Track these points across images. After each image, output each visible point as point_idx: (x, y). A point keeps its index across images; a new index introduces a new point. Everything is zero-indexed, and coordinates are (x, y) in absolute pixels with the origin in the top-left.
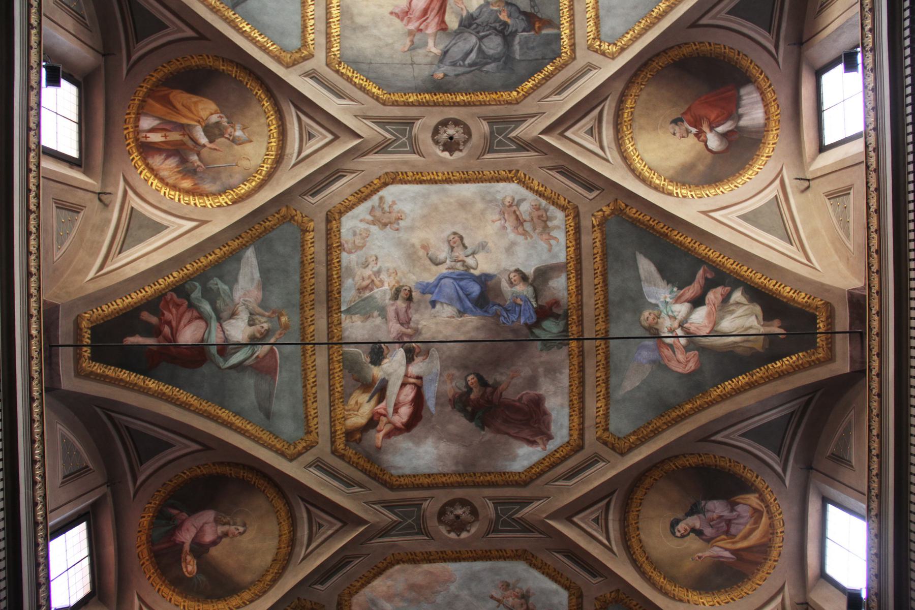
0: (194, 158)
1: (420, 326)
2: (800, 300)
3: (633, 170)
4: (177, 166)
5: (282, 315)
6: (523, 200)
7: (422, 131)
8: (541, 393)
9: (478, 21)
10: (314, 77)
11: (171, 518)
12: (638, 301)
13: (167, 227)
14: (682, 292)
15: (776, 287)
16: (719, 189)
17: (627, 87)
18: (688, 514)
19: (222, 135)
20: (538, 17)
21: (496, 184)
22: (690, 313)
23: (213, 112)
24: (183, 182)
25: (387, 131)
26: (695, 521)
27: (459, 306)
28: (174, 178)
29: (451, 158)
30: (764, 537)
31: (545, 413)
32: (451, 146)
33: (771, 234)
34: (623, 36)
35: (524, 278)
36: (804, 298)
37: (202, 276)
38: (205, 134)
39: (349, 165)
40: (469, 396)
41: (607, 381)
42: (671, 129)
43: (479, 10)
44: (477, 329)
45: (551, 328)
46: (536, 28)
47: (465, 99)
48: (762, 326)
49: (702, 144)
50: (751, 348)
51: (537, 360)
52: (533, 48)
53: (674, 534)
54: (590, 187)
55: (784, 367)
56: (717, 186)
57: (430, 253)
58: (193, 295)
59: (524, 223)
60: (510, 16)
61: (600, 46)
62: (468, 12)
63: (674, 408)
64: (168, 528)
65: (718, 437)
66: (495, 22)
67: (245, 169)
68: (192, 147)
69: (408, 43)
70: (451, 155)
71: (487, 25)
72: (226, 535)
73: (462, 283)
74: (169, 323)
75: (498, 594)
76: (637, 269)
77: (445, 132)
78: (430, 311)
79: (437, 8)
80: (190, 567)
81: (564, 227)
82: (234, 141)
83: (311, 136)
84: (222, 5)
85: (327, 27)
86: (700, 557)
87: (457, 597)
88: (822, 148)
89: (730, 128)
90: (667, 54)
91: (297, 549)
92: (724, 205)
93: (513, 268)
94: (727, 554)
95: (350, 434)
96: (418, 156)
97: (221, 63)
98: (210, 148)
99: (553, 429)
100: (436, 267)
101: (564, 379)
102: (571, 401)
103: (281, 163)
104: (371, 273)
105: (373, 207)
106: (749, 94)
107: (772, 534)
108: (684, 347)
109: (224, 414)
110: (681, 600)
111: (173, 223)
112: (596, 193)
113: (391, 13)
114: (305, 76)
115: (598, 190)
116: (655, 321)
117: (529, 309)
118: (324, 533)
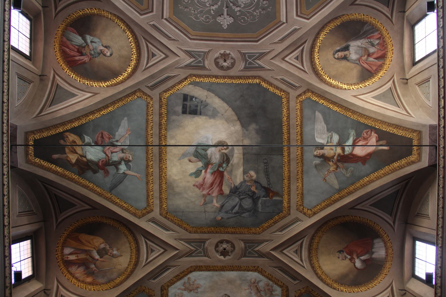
0: (93, 266)
3: (317, 274)
4: (84, 271)
6: (260, 281)
7: (210, 245)
9: (240, 190)
10: (154, 221)
16: (360, 289)
17: (316, 232)
19: (107, 254)
20: (271, 190)
21: (247, 272)
23: (101, 243)
24: (87, 279)
29: (224, 259)
32: (224, 253)
34: (315, 207)
39: (172, 263)
42: (337, 254)
46: (270, 196)
49: (353, 264)
54: (295, 279)
56: (359, 287)
59: (261, 292)
60: (256, 188)
61: (303, 209)
66: (248, 191)
67: (119, 270)
68: (91, 261)
69: (203, 201)
70: (224, 258)
71: (244, 193)
77: (222, 246)
79: (218, 183)
82: (113, 256)
83: (152, 251)
84: (104, 191)
85: (160, 195)
88: (414, 63)
89: (368, 258)
90: (337, 219)
96: (207, 258)
98: (101, 261)
105: (185, 283)
113: (194, 185)
114: (149, 222)
115: (299, 280)
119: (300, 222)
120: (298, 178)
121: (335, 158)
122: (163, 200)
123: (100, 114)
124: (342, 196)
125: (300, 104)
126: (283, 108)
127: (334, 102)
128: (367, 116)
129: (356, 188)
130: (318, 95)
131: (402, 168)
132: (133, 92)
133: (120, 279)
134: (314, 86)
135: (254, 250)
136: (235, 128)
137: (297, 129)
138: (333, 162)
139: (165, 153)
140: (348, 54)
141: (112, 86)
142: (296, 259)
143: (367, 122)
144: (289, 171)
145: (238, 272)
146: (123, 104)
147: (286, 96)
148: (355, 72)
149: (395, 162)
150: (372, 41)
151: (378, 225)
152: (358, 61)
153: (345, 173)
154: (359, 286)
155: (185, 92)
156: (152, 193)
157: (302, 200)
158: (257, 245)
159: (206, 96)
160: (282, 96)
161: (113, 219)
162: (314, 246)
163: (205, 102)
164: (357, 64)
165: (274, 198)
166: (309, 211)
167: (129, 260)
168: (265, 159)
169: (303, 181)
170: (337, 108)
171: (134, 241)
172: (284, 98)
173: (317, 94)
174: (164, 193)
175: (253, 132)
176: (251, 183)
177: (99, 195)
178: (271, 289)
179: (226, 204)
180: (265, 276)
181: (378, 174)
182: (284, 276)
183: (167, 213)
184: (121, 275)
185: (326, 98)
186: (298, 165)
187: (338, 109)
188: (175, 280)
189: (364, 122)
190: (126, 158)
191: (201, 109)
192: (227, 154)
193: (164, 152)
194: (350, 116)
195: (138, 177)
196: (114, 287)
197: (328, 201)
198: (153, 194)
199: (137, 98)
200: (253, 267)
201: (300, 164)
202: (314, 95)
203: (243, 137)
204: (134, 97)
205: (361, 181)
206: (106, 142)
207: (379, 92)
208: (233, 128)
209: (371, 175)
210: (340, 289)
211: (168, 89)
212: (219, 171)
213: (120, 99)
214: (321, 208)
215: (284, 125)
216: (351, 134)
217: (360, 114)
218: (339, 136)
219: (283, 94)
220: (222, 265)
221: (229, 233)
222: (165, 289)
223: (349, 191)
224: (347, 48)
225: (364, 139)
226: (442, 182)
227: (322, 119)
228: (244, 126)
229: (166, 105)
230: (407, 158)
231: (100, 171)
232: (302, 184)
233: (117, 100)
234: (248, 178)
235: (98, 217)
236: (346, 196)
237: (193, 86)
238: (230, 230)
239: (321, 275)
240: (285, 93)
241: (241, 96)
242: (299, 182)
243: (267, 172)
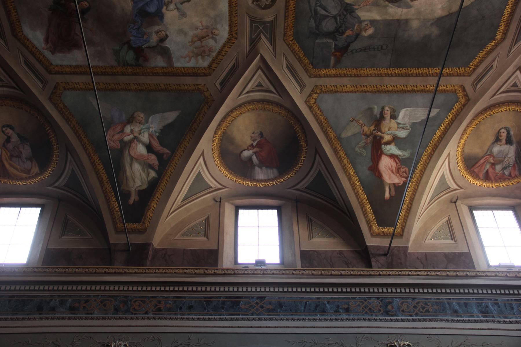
2: (149, 213)
3: (232, 111)
6: (216, 40)
9: (348, 16)
14: (156, 139)
15: (157, 198)
16: (217, 158)
17: (286, 109)
18: (19, 136)
21: (228, 24)
26: (15, 138)
34: (319, 108)
35: (162, 40)
36: (150, 215)
45: (130, 56)
47: (291, 6)
48: (135, 189)
55: (113, 203)
61: (316, 93)
62: (356, 9)
65: (69, 157)
71: (344, 21)
81: (197, 66)
89: (254, 162)
92: (207, 163)
93: (168, 33)
102: (81, 66)
108: (123, 139)
112: (219, 87)
115: (221, 89)
116: (138, 121)
119: (299, 91)
120: (357, 87)
121: (378, 133)
124: (332, 141)
125: (452, 90)
126: (453, 68)
127: (446, 132)
128: (424, 172)
129: (341, 159)
130: (459, 112)
131: (364, 215)
135: (261, 34)
136: (439, 9)
137: (420, 85)
138: (374, 130)
140: (501, 143)
142: (250, 85)
143: (417, 172)
144: (368, 76)
148: (476, 150)
149: (371, 206)
150: (509, 168)
152: (490, 154)
154: (221, 157)
157: (328, 91)
158: (269, 37)
160: (469, 67)
162: (268, 106)
164: (487, 152)
166: (314, 100)
168: (387, 47)
169: (353, 93)
170: (438, 136)
172: (465, 70)
173: (461, 111)
178: (205, 54)
181: (358, 186)
182: (224, 71)
186: (374, 87)
187: (438, 137)
189: (417, 168)
194: (426, 150)
197: (326, 124)
200: (236, 32)
201: (374, 90)
202: (461, 107)
205: (349, 166)
207: (448, 178)
208: (439, 6)
209: (357, 178)
210: (215, 139)
214: (317, 115)
215: (428, 69)
216: (405, 152)
217: (428, 164)
223: (339, 150)
224: (509, 141)
225: (398, 168)
226: (357, 273)
228: (439, 21)
230: (375, 220)
232: (348, 92)
234: (365, 26)
236: (332, 146)
240: (471, 71)
242: (351, 87)
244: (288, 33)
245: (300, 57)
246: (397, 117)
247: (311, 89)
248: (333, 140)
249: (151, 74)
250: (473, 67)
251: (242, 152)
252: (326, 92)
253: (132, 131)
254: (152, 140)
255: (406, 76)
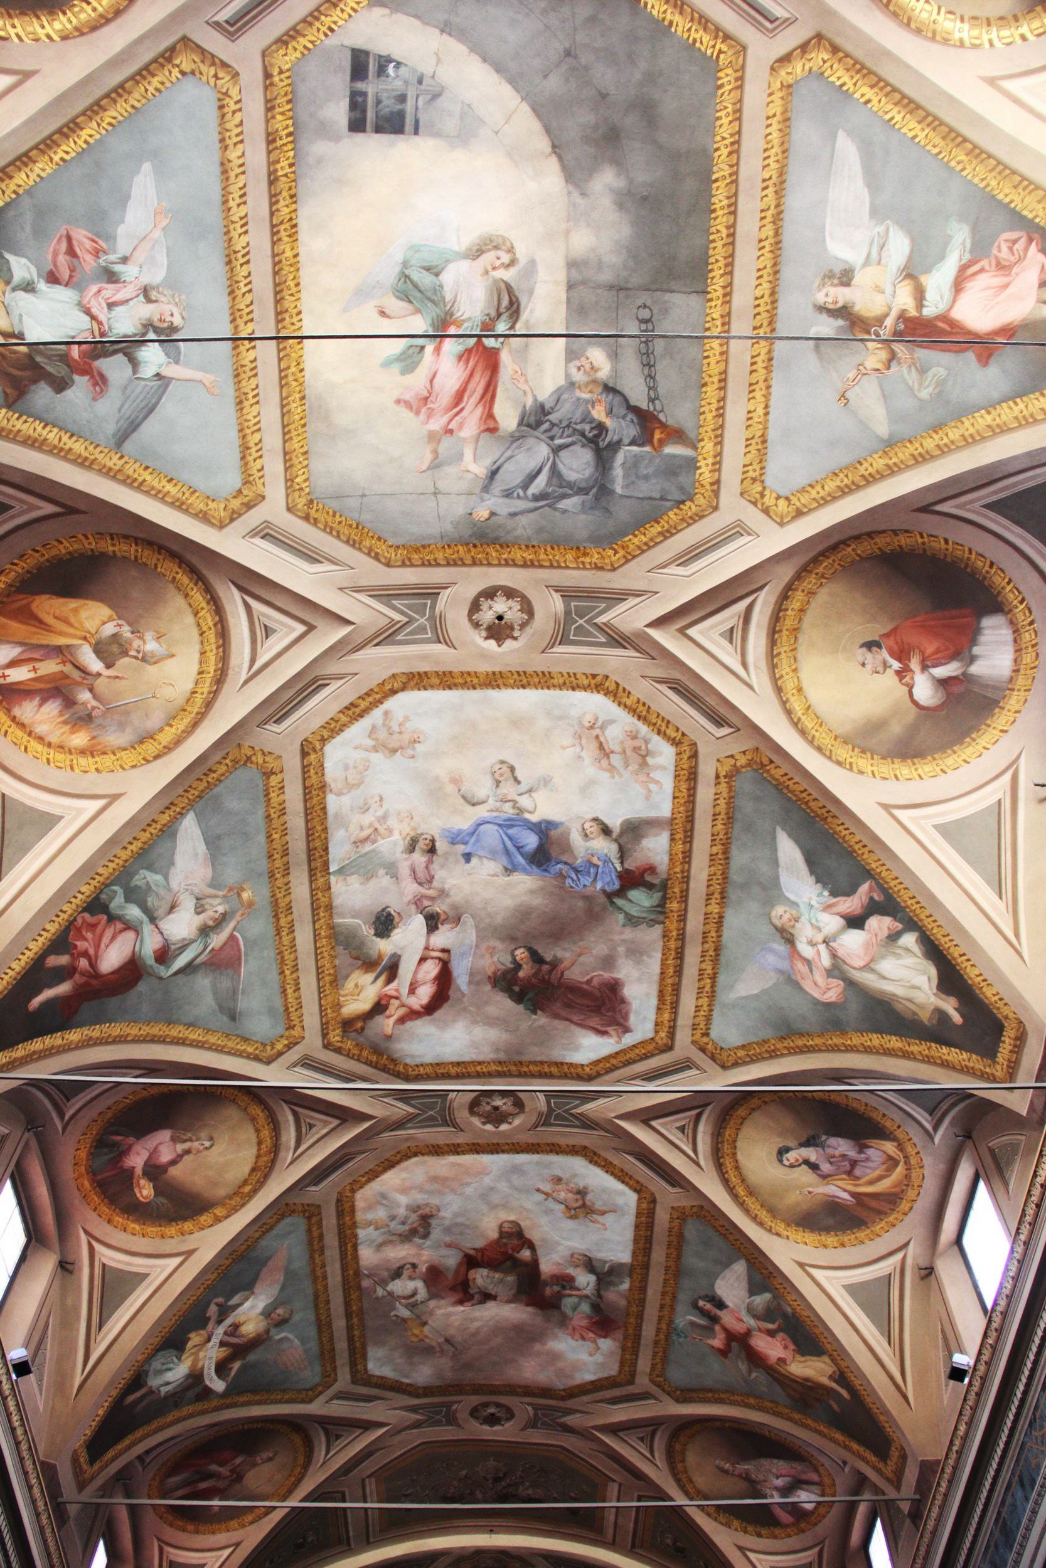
1: (447, 886)
4: (61, 714)
5: (243, 890)
6: (611, 722)
8: (619, 976)
9: (553, 417)
10: (267, 534)
11: (114, 1145)
12: (771, 891)
13: (60, 818)
14: (835, 900)
17: (798, 577)
18: (802, 1145)
19: (125, 653)
20: (660, 422)
21: (570, 692)
22: (841, 931)
23: (105, 619)
24: (74, 736)
25: (394, 608)
26: (811, 1154)
27: (505, 861)
28: (58, 733)
30: (896, 1186)
31: (623, 1001)
32: (499, 631)
33: (975, 869)
35: (606, 831)
37: (123, 877)
38: (98, 656)
39: (333, 668)
40: (517, 973)
41: (714, 978)
43: (555, 396)
44: (532, 892)
45: (641, 899)
50: (915, 1013)
51: (616, 937)
52: (646, 478)
53: (781, 1161)
54: (719, 721)
57: (463, 789)
58: (112, 906)
60: (610, 412)
61: (762, 496)
62: (535, 400)
63: (801, 1035)
64: (111, 1156)
68: (80, 680)
69: (429, 456)
70: (499, 646)
71: (568, 426)
72: (188, 1152)
73: (510, 832)
74: (85, 954)
75: (547, 1187)
76: (774, 849)
77: (490, 608)
78: (462, 866)
80: (145, 1191)
81: (672, 768)
83: (268, 632)
84: (99, 449)
86: (810, 1193)
87: (492, 1189)
91: (282, 1154)
94: (846, 1196)
95: (347, 1024)
96: (444, 647)
97: (109, 541)
98: (109, 677)
99: (633, 1020)
100: (472, 808)
101: (654, 964)
103: (224, 681)
104: (373, 819)
105: (374, 728)
106: (993, 628)
107: (907, 1185)
109: (174, 1032)
110: (778, 1234)
111: (70, 808)
112: (726, 730)
113: (398, 402)
114: (252, 537)
115: (731, 727)
116: (792, 923)
117: (610, 872)
118: (317, 1133)
119: (751, 538)
122: (294, 458)
123: (51, 160)
124: (895, 464)
125: (782, 98)
129: (945, 445)
130: (854, 65)
132: (162, 55)
133: (173, 730)
134: (844, 21)
139: (294, 290)
141: (82, 34)
145: (540, 691)
146: (133, 107)
147: (733, 59)
151: (1003, 571)
153: (916, 386)
155: (360, 43)
156: (257, 436)
159: (436, 54)
160: (718, 57)
161: (137, 540)
163: (431, 82)
165: (670, 450)
167: (196, 667)
168: (645, 306)
171: (208, 603)
172: (727, 67)
174: (299, 435)
175: (607, 202)
176: (591, 392)
177: (84, 463)
178: (643, 747)
179: (506, 466)
180: (625, 706)
181: (1026, 407)
183: (311, 501)
184: (174, 718)
185: (884, 80)
188: (344, 719)
189: (1007, 200)
190: (160, 320)
191: (417, 108)
192: (513, 285)
193: (292, 284)
194: (959, 167)
195: (207, 384)
196: (157, 757)
197: (847, 476)
198: (260, 441)
199: (179, 76)
202: (840, 60)
203: (568, 221)
204: (170, 72)
206: (87, 269)
209: (1004, 405)
211: (294, 28)
212: (484, 347)
213: (120, 91)
214: (822, 498)
215: (716, 180)
216: (953, 241)
218: (913, 240)
219: (724, 48)
220: (490, 669)
221: (515, 565)
222: (315, 750)
227: (857, 168)
229: (290, 97)
231: (76, 377)
233: (107, 96)
234: (581, 372)
235: (87, 538)
237: (387, 11)
238: (518, 555)
239: (803, 718)
240: (730, 47)
241: (568, 53)
242: (754, 398)
243: (647, 354)
244: (594, 560)
245: (659, 533)
246: (847, 267)
247: (752, 507)
248: (891, 462)
249: (686, 866)
250: (719, 41)
251: (915, 703)
252: (762, 468)
253: (812, 943)
254: (835, 910)
255: (733, 243)
